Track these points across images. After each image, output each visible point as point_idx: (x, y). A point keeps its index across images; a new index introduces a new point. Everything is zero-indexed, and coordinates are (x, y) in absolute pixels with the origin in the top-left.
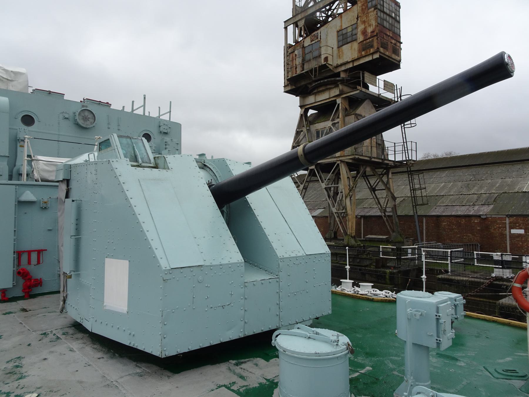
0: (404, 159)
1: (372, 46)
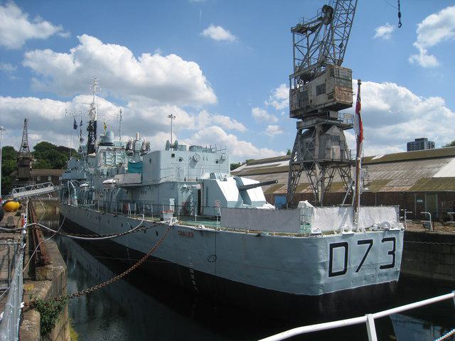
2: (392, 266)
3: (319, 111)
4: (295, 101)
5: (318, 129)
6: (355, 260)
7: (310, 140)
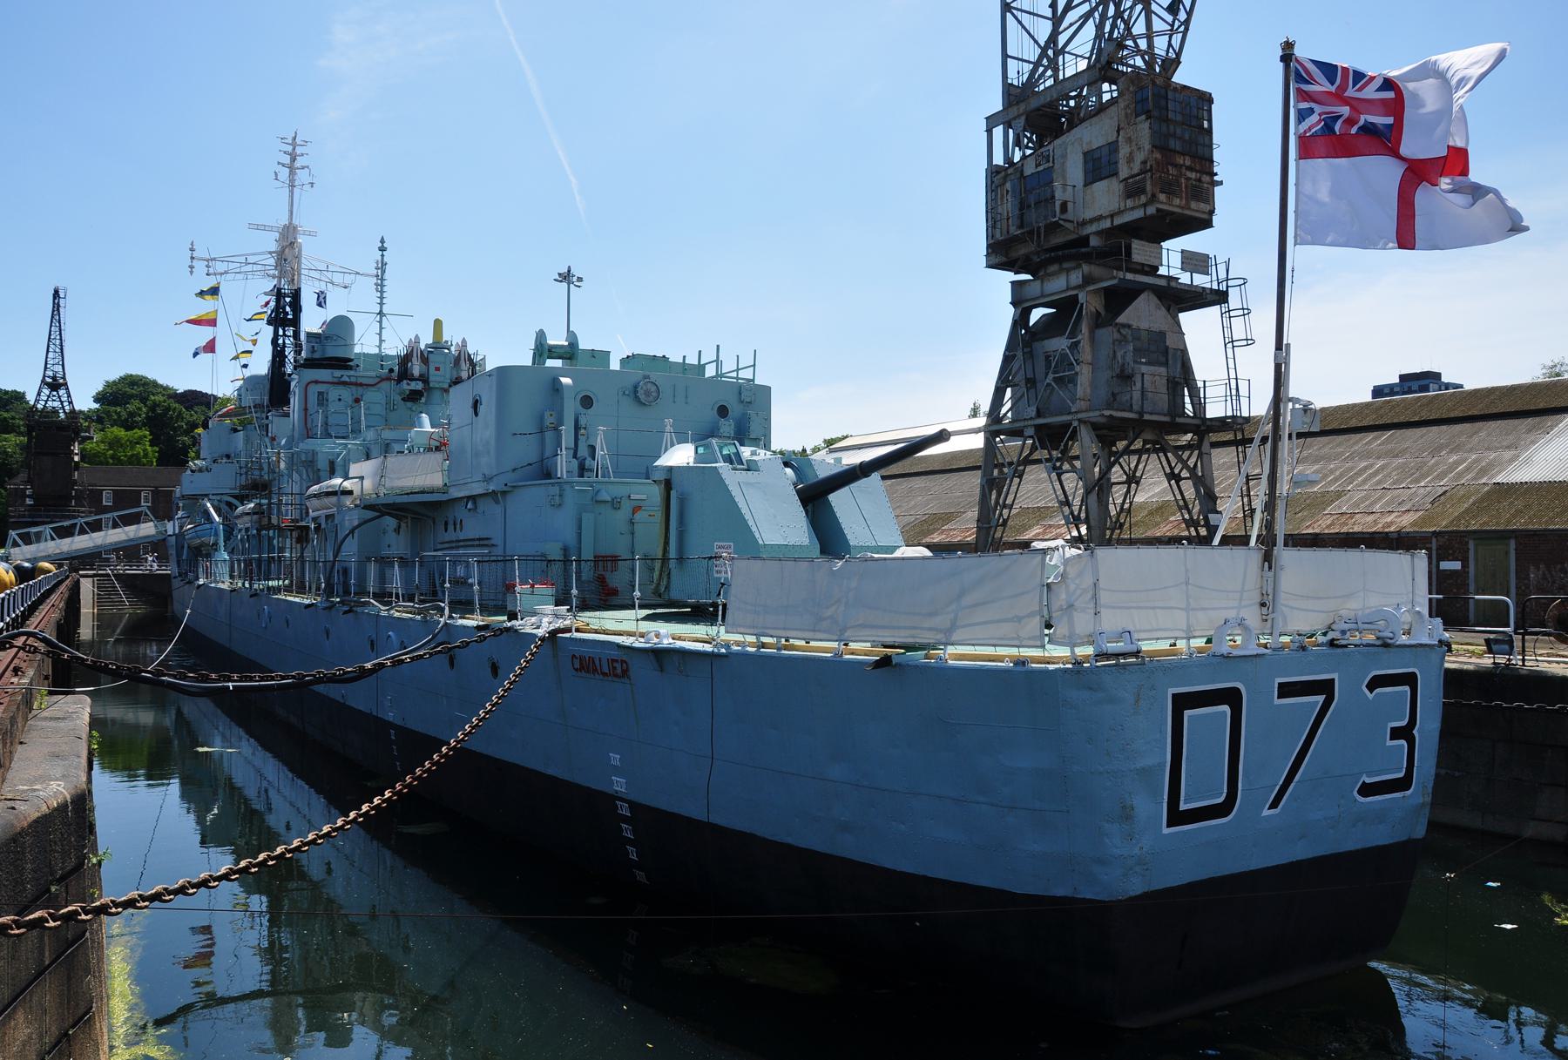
0: (1229, 413)
1: (1143, 191)
2: (1403, 784)
3: (1094, 242)
4: (1008, 206)
5: (1090, 302)
6: (1265, 761)
7: (1059, 344)
